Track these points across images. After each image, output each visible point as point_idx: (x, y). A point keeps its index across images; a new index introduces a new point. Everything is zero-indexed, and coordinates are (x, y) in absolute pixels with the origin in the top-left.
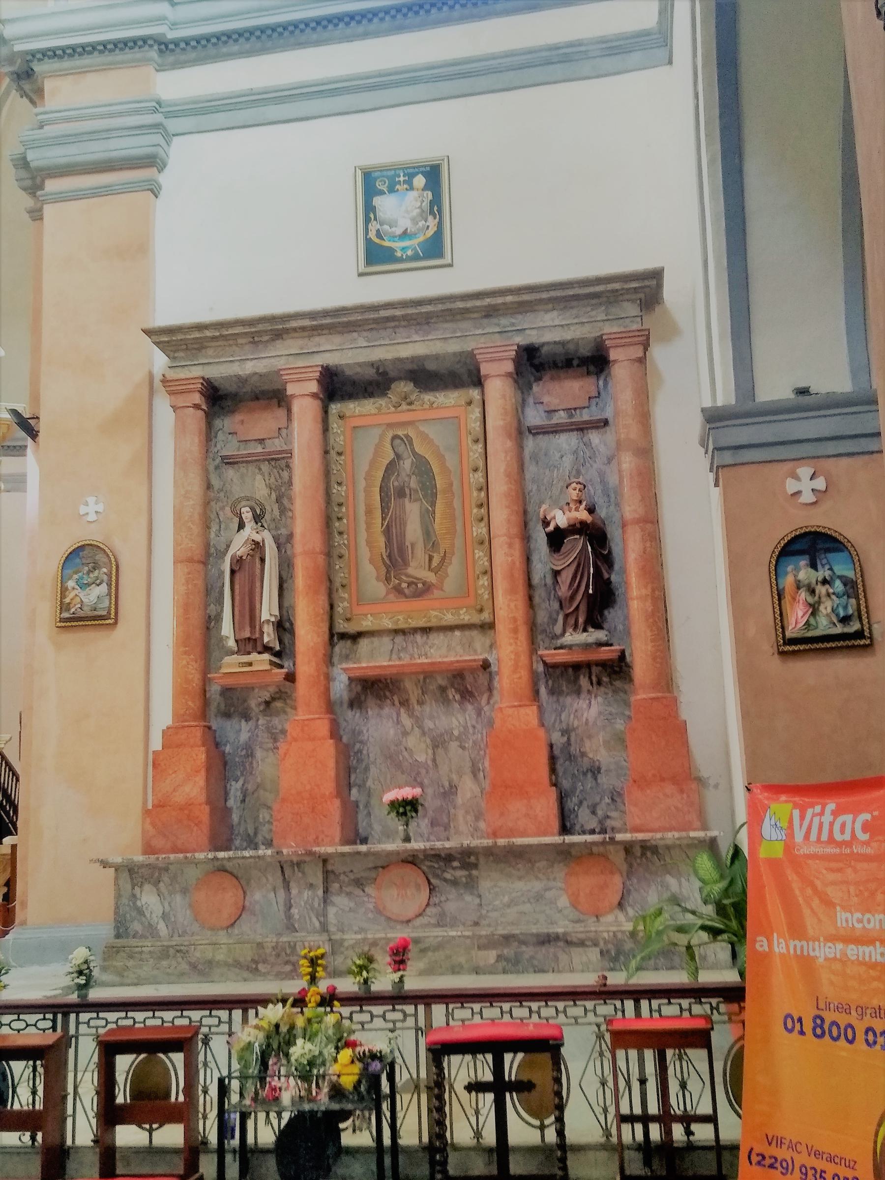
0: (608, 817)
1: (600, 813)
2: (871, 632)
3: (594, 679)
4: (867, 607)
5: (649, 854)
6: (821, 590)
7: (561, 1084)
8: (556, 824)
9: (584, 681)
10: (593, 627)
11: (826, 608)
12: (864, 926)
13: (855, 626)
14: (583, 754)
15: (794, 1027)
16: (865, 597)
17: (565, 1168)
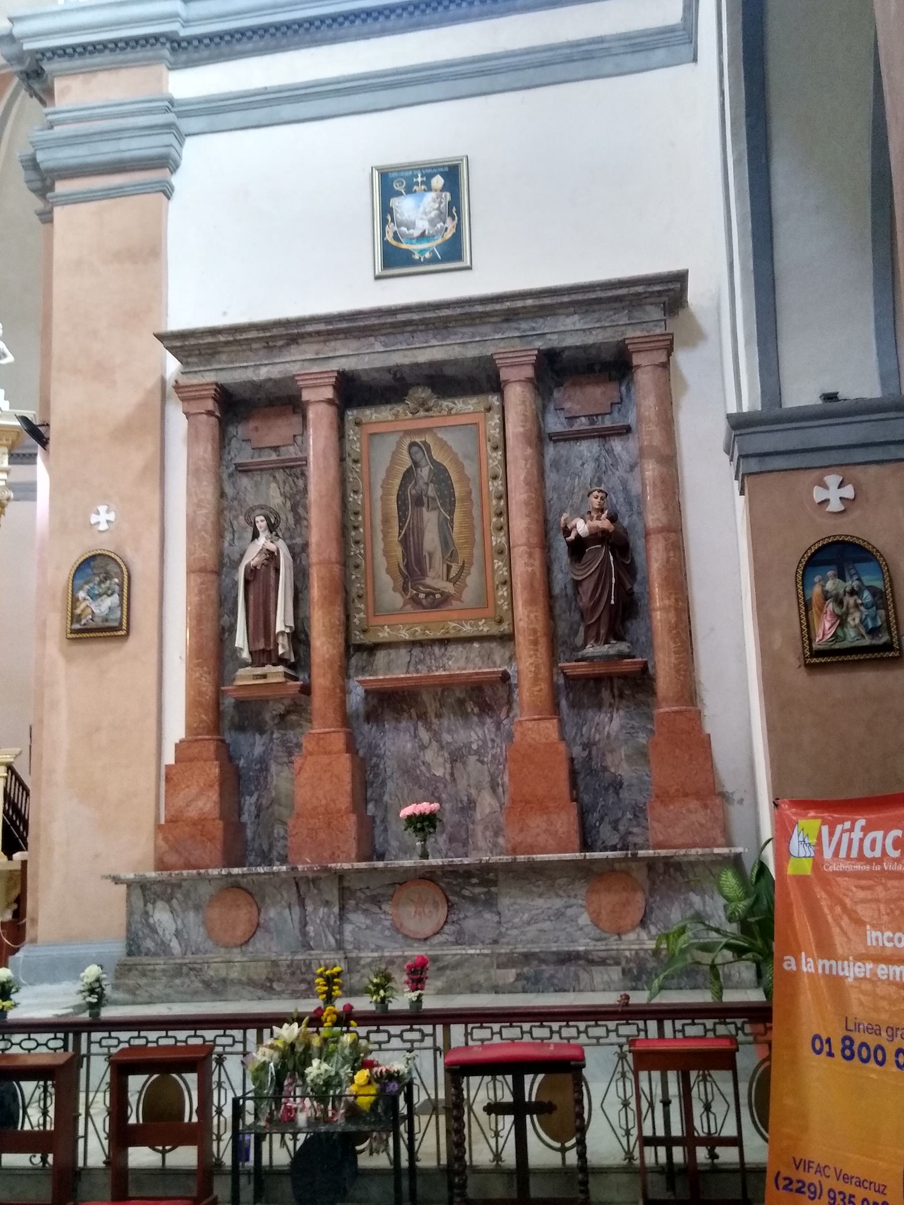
0: (631, 833)
3: (616, 692)
4: (896, 618)
6: (850, 601)
8: (576, 841)
9: (606, 694)
10: (615, 639)
11: (854, 619)
13: (884, 638)
14: (605, 769)
17: (586, 1192)
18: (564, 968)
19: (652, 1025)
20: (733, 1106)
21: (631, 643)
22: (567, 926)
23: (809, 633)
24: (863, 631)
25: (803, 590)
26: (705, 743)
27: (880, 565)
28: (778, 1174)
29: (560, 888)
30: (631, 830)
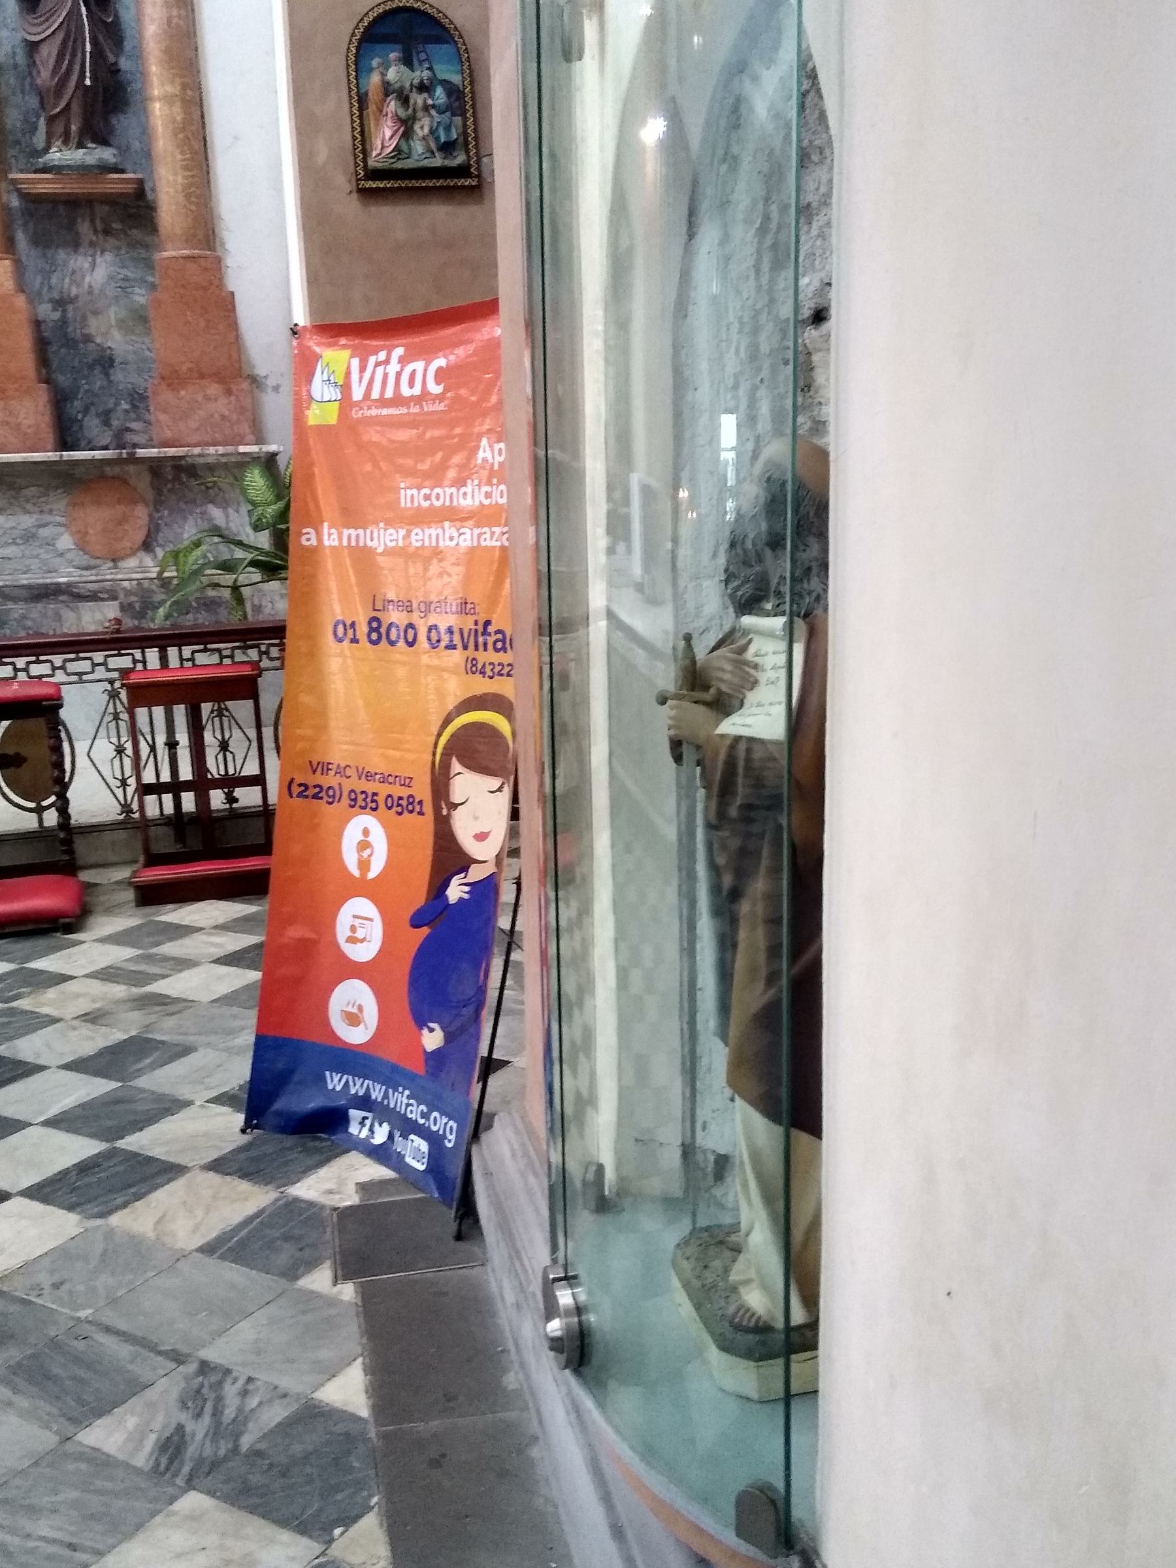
0: (128, 430)
1: (115, 423)
2: (478, 169)
3: (99, 226)
4: (475, 130)
5: (184, 477)
6: (418, 99)
7: (62, 756)
8: (49, 437)
9: (84, 228)
10: (93, 141)
11: (422, 127)
12: (432, 504)
13: (459, 159)
14: (88, 339)
15: (345, 634)
16: (474, 115)
17: (71, 852)
18: (40, 606)
19: (153, 655)
20: (255, 744)
21: (118, 148)
22: (42, 551)
23: (363, 142)
24: (433, 145)
25: (357, 78)
26: (227, 305)
27: (458, 50)
28: (292, 781)
29: (28, 501)
30: (128, 425)
